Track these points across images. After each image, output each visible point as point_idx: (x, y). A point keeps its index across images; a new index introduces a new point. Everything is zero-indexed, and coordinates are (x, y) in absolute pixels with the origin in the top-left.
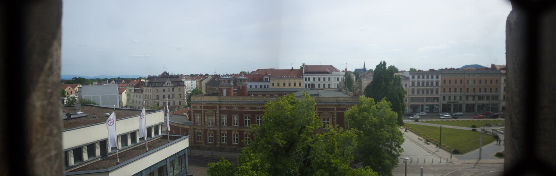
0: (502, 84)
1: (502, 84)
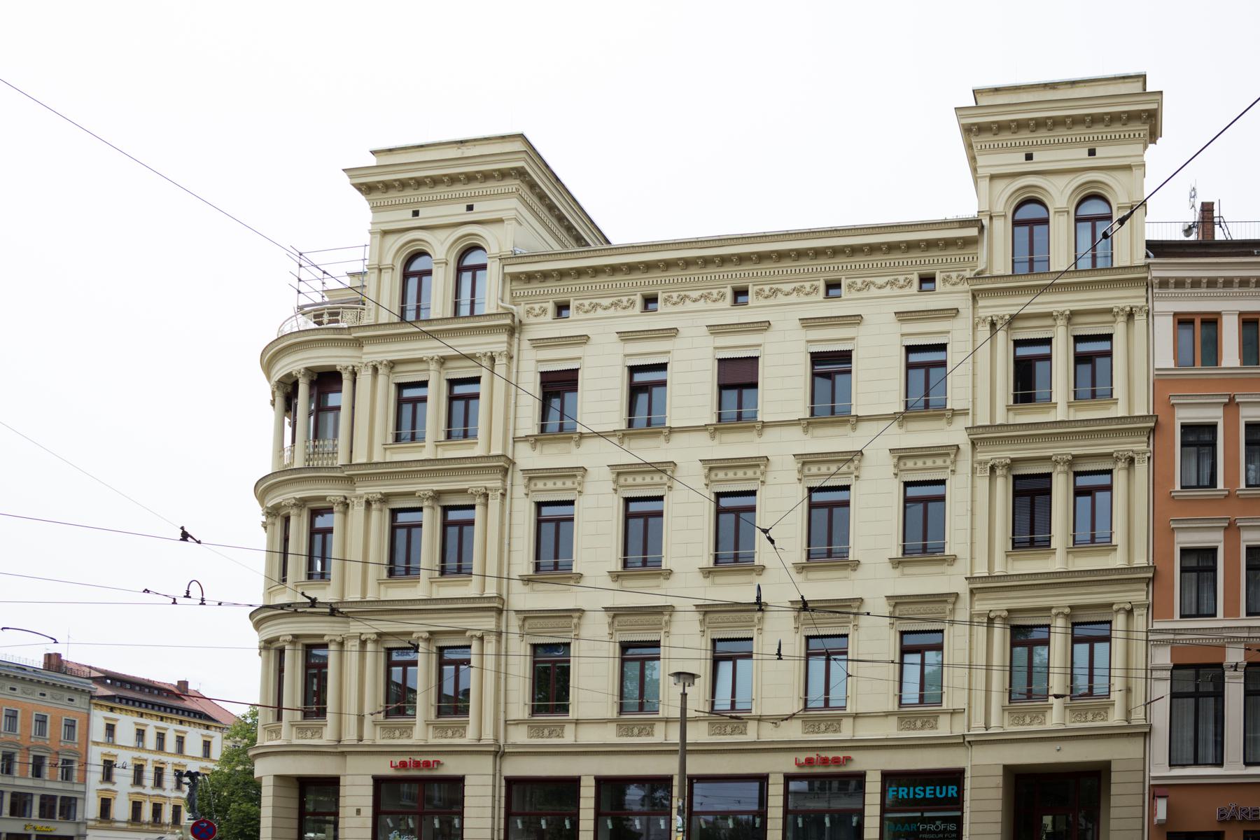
0: (97, 743)
1: (97, 743)
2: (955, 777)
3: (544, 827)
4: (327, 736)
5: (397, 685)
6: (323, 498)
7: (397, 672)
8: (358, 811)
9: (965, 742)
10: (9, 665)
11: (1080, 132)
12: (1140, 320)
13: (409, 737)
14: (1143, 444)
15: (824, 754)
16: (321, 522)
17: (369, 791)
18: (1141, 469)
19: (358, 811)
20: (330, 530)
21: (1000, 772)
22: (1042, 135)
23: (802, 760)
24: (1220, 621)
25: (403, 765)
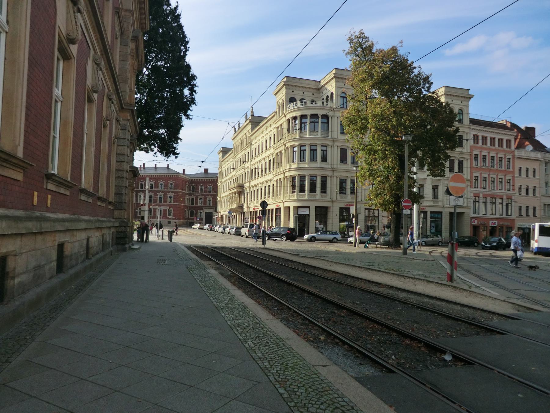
2: (441, 213)
3: (36, 193)
4: (328, 198)
5: (60, 182)
6: (294, 145)
7: (302, 183)
8: (336, 215)
9: (443, 207)
10: (1, 174)
11: (460, 98)
12: (468, 134)
13: (346, 199)
14: (69, 168)
15: (350, 204)
16: (303, 148)
17: (339, 210)
18: (469, 161)
19: (336, 215)
20: (305, 150)
21: (449, 213)
22: (455, 98)
23: (346, 205)
24: (479, 189)
25: (347, 205)
